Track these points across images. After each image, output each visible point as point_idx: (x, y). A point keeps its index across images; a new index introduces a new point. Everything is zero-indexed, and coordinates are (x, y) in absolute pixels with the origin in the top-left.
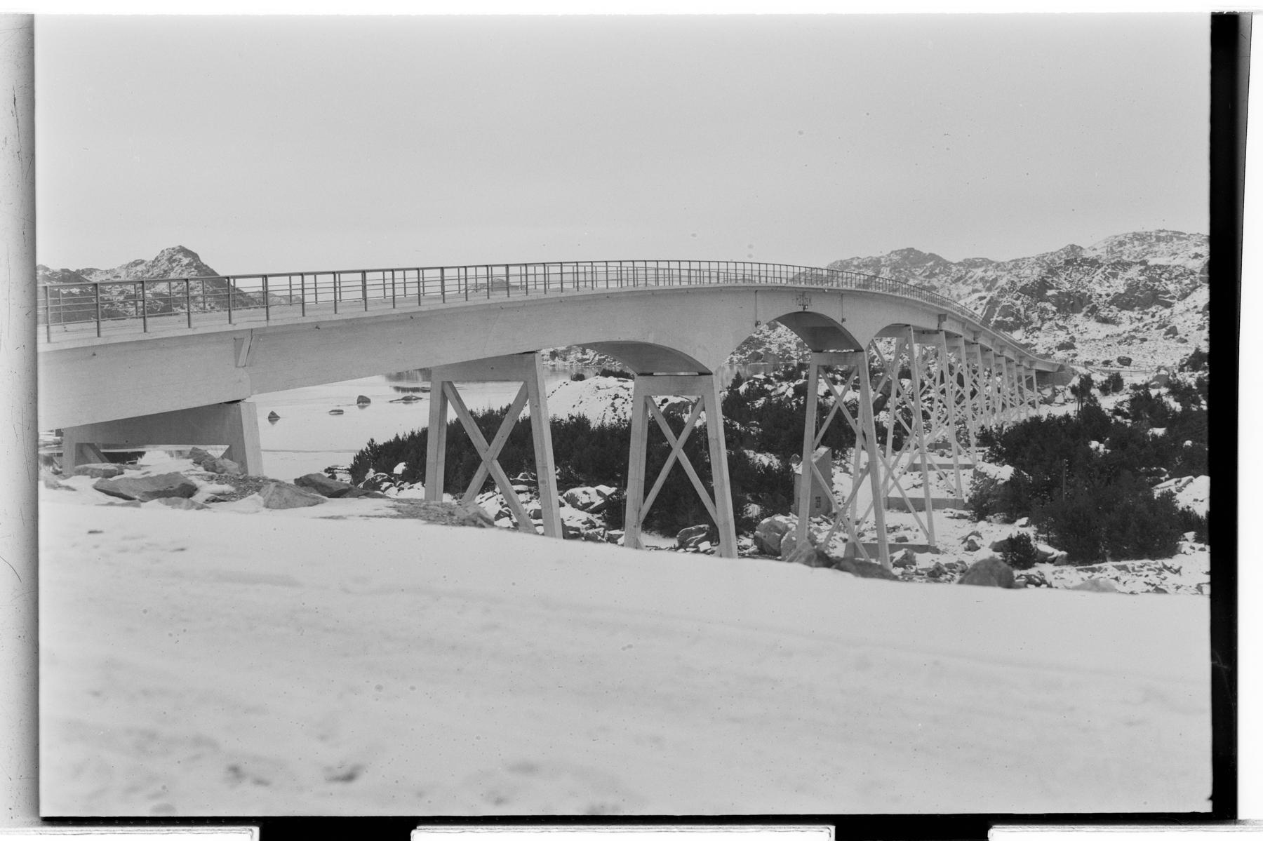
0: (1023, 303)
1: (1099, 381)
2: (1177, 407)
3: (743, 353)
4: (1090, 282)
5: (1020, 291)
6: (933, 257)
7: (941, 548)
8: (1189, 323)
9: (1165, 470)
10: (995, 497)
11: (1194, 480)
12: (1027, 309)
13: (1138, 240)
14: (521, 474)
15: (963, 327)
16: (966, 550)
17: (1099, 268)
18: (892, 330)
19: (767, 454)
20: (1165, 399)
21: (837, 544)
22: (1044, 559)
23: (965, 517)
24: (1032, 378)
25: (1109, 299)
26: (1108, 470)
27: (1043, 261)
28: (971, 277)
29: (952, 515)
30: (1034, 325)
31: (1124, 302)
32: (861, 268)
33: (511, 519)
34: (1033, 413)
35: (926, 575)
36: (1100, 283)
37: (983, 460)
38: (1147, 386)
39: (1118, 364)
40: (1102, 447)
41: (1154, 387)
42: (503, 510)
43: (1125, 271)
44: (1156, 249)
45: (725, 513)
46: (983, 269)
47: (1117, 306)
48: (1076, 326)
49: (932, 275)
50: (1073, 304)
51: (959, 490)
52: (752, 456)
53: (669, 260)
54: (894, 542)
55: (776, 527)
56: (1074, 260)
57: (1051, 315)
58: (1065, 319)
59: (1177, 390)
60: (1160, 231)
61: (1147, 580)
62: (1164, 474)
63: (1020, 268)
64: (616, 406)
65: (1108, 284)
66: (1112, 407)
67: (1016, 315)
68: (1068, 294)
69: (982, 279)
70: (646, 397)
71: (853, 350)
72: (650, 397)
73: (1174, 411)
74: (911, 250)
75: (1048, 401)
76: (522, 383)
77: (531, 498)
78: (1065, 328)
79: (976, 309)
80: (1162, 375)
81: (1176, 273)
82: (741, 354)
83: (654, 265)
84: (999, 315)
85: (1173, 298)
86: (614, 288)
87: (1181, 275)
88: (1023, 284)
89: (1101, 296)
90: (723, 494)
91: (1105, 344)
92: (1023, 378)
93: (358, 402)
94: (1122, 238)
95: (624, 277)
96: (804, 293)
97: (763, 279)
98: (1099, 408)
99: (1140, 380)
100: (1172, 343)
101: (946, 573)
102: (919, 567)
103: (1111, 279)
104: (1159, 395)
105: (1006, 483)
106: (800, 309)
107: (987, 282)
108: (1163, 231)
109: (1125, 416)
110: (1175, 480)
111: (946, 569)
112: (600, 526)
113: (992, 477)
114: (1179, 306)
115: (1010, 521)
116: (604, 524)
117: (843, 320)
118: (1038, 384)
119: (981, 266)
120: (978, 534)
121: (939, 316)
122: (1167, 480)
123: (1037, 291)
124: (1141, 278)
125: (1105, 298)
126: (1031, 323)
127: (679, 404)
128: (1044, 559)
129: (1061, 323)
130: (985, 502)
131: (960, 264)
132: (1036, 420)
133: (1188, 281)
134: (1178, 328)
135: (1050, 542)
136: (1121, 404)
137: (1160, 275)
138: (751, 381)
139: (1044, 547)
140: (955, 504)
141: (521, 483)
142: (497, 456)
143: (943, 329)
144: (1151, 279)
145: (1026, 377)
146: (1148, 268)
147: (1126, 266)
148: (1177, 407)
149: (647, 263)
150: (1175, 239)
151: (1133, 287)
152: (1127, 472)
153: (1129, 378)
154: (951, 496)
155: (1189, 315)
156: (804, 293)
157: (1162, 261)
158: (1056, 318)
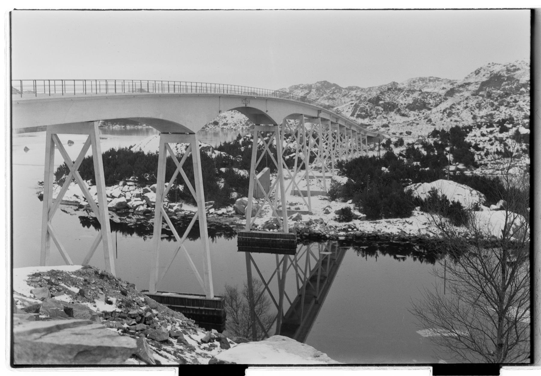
0: (369, 107)
1: (394, 141)
2: (425, 153)
3: (248, 125)
4: (398, 98)
5: (368, 101)
6: (335, 85)
7: (313, 212)
8: (437, 117)
9: (411, 180)
10: (340, 191)
11: (422, 185)
12: (371, 109)
13: (421, 80)
14: (132, 177)
15: (330, 116)
16: (324, 213)
17: (402, 92)
18: (294, 116)
19: (244, 170)
20: (420, 149)
21: (269, 210)
22: (356, 218)
23: (326, 199)
24: (365, 140)
25: (405, 106)
26: (387, 179)
27: (381, 89)
28: (350, 95)
29: (321, 198)
30: (373, 116)
31: (411, 107)
32: (303, 89)
33: (125, 197)
34: (364, 154)
35: (305, 225)
36: (402, 99)
37: (337, 175)
38: (413, 144)
39: (406, 135)
40: (387, 169)
41: (416, 144)
42: (122, 194)
43: (413, 94)
44: (428, 85)
45: (200, 196)
46: (356, 91)
47: (409, 109)
48: (391, 117)
49: (334, 93)
50: (390, 108)
51: (325, 187)
52: (237, 171)
53: (21, 79)
54: (294, 210)
55: (243, 203)
56: (393, 88)
57: (381, 112)
58: (387, 114)
59: (426, 146)
60: (431, 77)
61: (398, 227)
62: (410, 182)
63: (371, 91)
64: (178, 147)
65: (405, 99)
66: (398, 153)
67: (366, 112)
68: (388, 103)
69: (355, 95)
70: (165, 144)
71: (272, 125)
72: (168, 144)
73: (424, 155)
74: (325, 82)
75: (372, 150)
76: (88, 135)
77: (135, 188)
78: (387, 118)
79: (349, 108)
80: (420, 140)
81: (434, 95)
82: (247, 125)
83: (195, 85)
84: (359, 111)
85: (432, 106)
86: (120, 93)
87: (436, 96)
88: (369, 98)
89: (402, 104)
90: (199, 188)
91: (402, 125)
92: (361, 139)
93: (68, 143)
94: (415, 80)
95: (157, 88)
96: (246, 98)
97: (229, 91)
98: (393, 153)
99: (411, 141)
100: (429, 126)
101: (314, 224)
102: (303, 221)
103: (406, 97)
104: (418, 148)
105: (344, 185)
106: (244, 106)
107: (357, 97)
108: (432, 77)
109: (404, 156)
110: (414, 184)
111: (314, 222)
112: (166, 201)
113: (339, 182)
114: (434, 110)
115: (345, 201)
116: (168, 200)
117: (267, 111)
118: (368, 142)
119: (355, 89)
120: (329, 207)
121: (318, 111)
122: (411, 184)
123: (375, 101)
124: (419, 97)
125: (404, 105)
126: (372, 115)
127: (206, 147)
128: (356, 218)
129: (385, 116)
130: (335, 193)
131: (346, 89)
132: (366, 158)
133: (438, 99)
134: (432, 119)
135: (360, 211)
136: (402, 151)
137: (427, 96)
138: (245, 138)
139: (357, 213)
140: (323, 193)
141: (131, 181)
142: (78, 168)
143: (320, 116)
144: (423, 98)
145: (362, 139)
146: (422, 93)
147: (413, 91)
148: (425, 153)
149: (56, 81)
150: (437, 81)
151: (415, 101)
152: (395, 181)
153: (407, 140)
154: (322, 190)
155: (437, 114)
156: (246, 98)
157: (429, 90)
158: (383, 113)
